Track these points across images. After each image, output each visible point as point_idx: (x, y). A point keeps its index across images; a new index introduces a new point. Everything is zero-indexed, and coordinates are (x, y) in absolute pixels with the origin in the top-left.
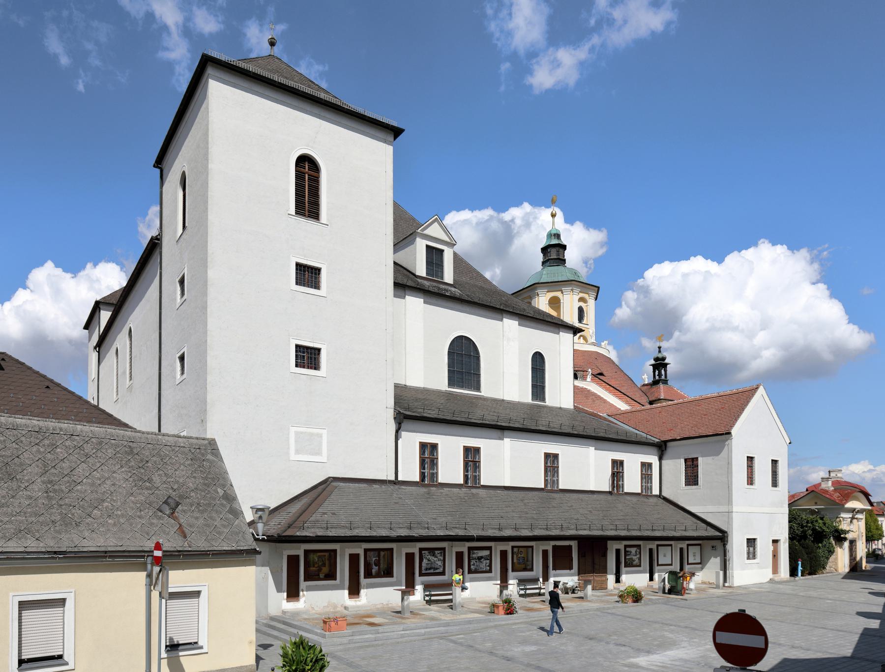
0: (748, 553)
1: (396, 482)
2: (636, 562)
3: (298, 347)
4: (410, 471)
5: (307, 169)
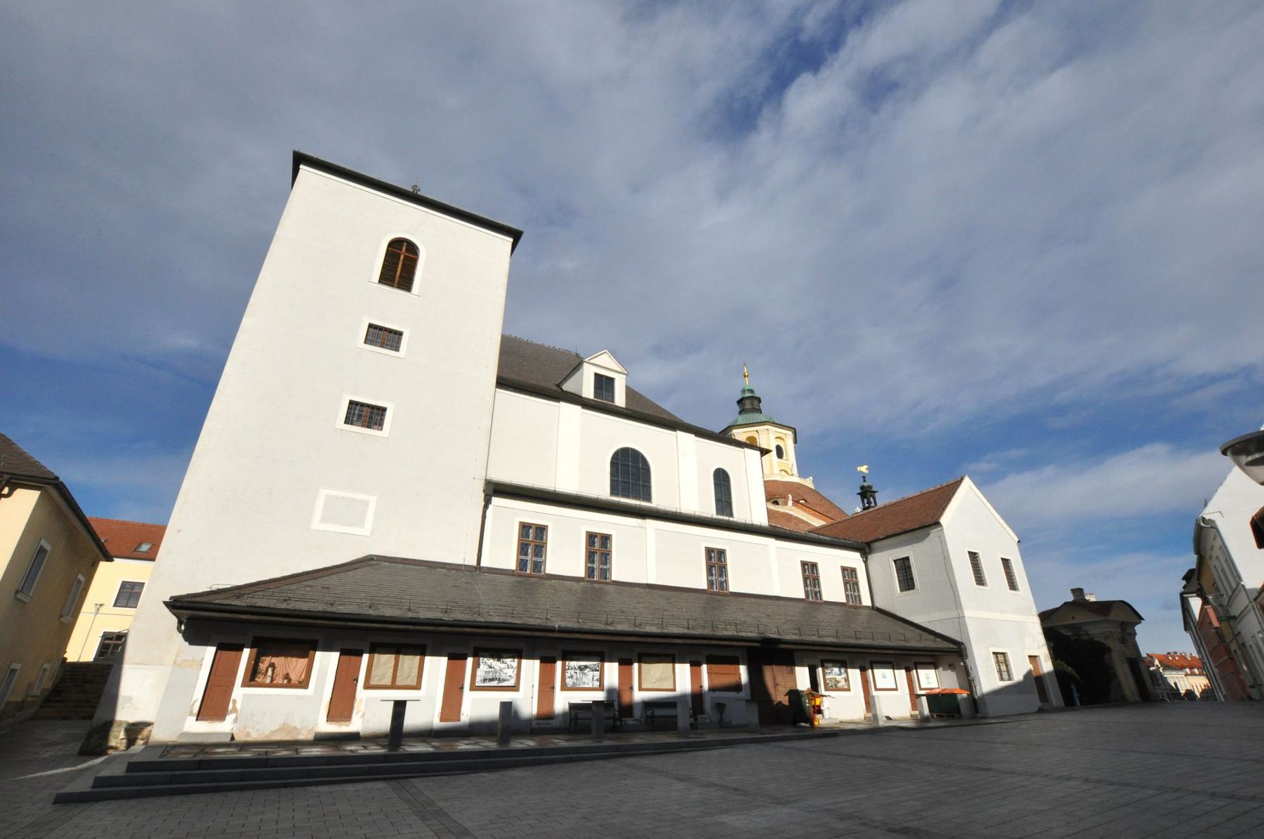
0: (1000, 672)
1: (478, 568)
2: (842, 684)
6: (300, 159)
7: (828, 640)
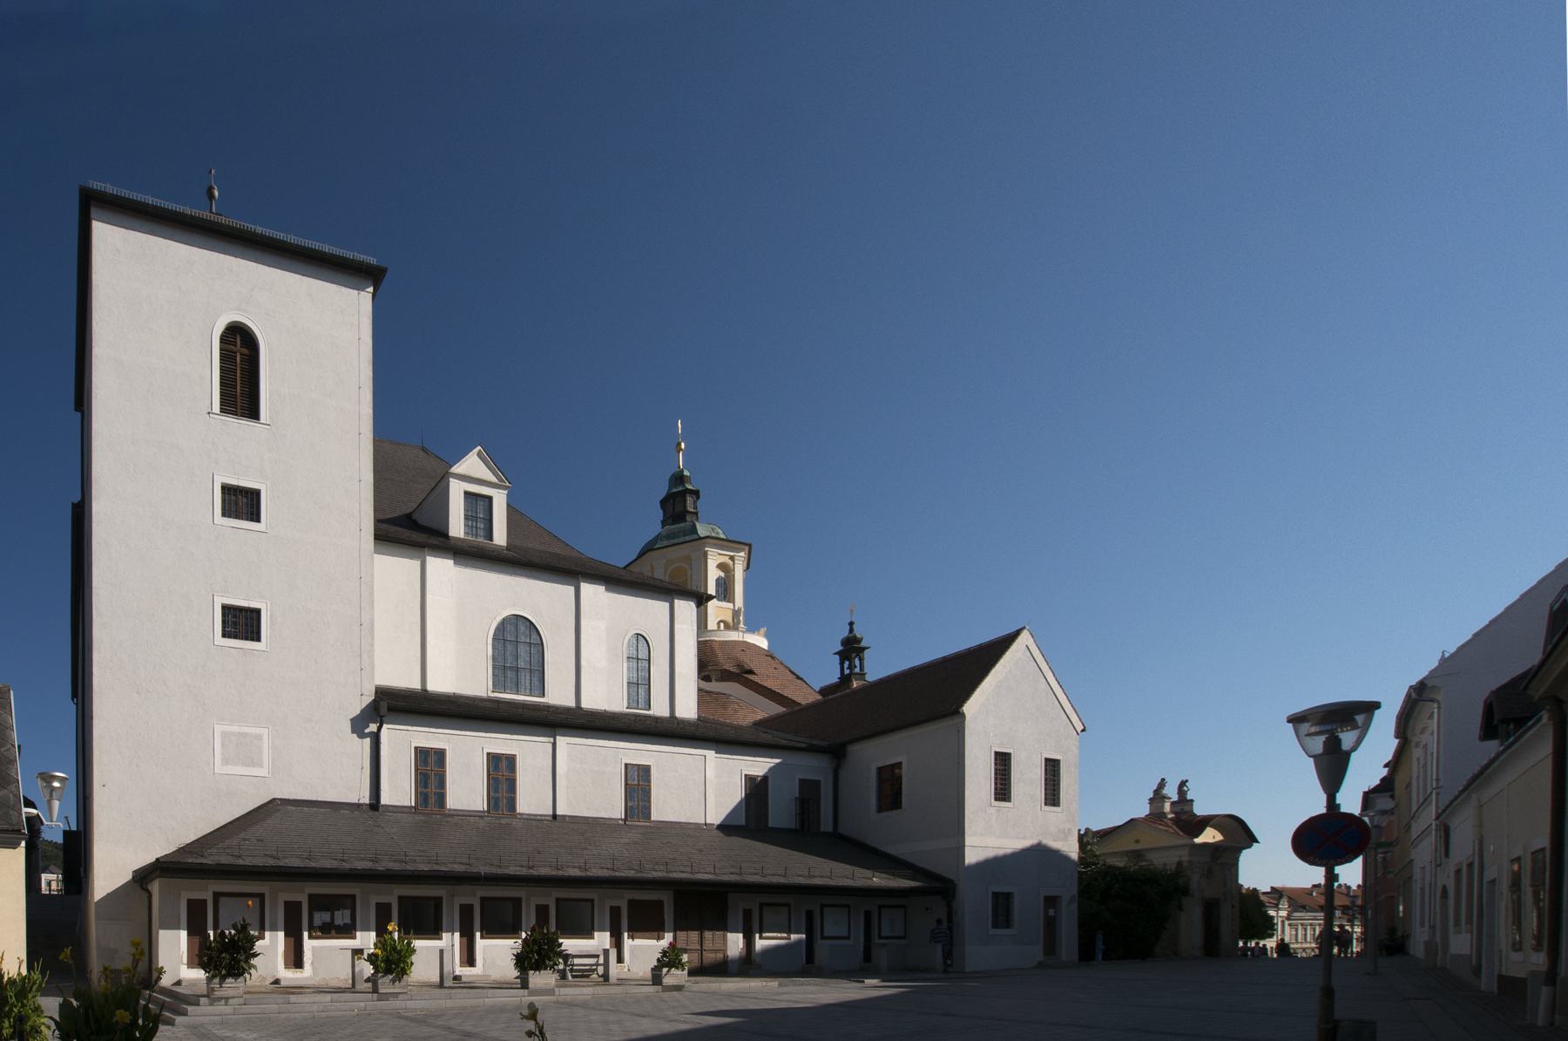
3: (226, 609)
4: (399, 790)
5: (240, 348)
6: (92, 203)
7: (775, 880)
